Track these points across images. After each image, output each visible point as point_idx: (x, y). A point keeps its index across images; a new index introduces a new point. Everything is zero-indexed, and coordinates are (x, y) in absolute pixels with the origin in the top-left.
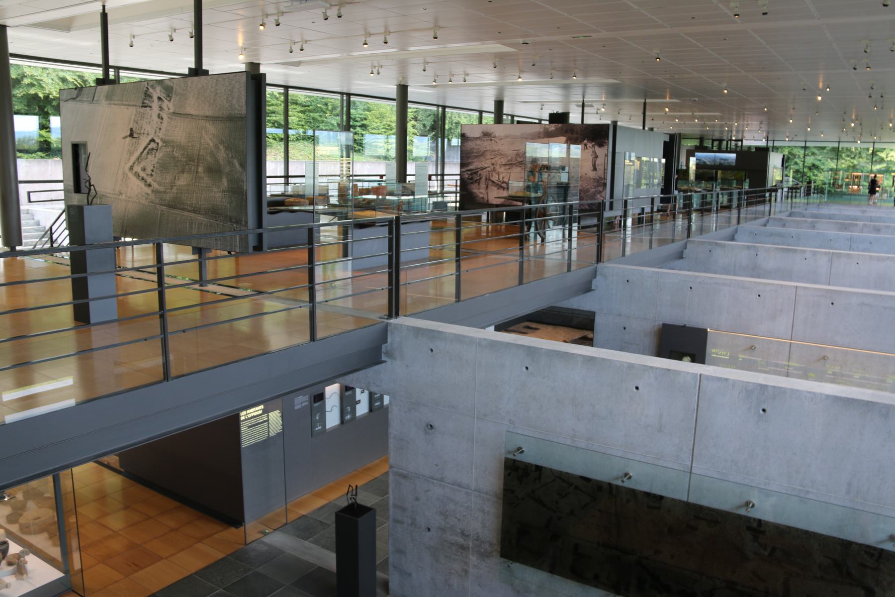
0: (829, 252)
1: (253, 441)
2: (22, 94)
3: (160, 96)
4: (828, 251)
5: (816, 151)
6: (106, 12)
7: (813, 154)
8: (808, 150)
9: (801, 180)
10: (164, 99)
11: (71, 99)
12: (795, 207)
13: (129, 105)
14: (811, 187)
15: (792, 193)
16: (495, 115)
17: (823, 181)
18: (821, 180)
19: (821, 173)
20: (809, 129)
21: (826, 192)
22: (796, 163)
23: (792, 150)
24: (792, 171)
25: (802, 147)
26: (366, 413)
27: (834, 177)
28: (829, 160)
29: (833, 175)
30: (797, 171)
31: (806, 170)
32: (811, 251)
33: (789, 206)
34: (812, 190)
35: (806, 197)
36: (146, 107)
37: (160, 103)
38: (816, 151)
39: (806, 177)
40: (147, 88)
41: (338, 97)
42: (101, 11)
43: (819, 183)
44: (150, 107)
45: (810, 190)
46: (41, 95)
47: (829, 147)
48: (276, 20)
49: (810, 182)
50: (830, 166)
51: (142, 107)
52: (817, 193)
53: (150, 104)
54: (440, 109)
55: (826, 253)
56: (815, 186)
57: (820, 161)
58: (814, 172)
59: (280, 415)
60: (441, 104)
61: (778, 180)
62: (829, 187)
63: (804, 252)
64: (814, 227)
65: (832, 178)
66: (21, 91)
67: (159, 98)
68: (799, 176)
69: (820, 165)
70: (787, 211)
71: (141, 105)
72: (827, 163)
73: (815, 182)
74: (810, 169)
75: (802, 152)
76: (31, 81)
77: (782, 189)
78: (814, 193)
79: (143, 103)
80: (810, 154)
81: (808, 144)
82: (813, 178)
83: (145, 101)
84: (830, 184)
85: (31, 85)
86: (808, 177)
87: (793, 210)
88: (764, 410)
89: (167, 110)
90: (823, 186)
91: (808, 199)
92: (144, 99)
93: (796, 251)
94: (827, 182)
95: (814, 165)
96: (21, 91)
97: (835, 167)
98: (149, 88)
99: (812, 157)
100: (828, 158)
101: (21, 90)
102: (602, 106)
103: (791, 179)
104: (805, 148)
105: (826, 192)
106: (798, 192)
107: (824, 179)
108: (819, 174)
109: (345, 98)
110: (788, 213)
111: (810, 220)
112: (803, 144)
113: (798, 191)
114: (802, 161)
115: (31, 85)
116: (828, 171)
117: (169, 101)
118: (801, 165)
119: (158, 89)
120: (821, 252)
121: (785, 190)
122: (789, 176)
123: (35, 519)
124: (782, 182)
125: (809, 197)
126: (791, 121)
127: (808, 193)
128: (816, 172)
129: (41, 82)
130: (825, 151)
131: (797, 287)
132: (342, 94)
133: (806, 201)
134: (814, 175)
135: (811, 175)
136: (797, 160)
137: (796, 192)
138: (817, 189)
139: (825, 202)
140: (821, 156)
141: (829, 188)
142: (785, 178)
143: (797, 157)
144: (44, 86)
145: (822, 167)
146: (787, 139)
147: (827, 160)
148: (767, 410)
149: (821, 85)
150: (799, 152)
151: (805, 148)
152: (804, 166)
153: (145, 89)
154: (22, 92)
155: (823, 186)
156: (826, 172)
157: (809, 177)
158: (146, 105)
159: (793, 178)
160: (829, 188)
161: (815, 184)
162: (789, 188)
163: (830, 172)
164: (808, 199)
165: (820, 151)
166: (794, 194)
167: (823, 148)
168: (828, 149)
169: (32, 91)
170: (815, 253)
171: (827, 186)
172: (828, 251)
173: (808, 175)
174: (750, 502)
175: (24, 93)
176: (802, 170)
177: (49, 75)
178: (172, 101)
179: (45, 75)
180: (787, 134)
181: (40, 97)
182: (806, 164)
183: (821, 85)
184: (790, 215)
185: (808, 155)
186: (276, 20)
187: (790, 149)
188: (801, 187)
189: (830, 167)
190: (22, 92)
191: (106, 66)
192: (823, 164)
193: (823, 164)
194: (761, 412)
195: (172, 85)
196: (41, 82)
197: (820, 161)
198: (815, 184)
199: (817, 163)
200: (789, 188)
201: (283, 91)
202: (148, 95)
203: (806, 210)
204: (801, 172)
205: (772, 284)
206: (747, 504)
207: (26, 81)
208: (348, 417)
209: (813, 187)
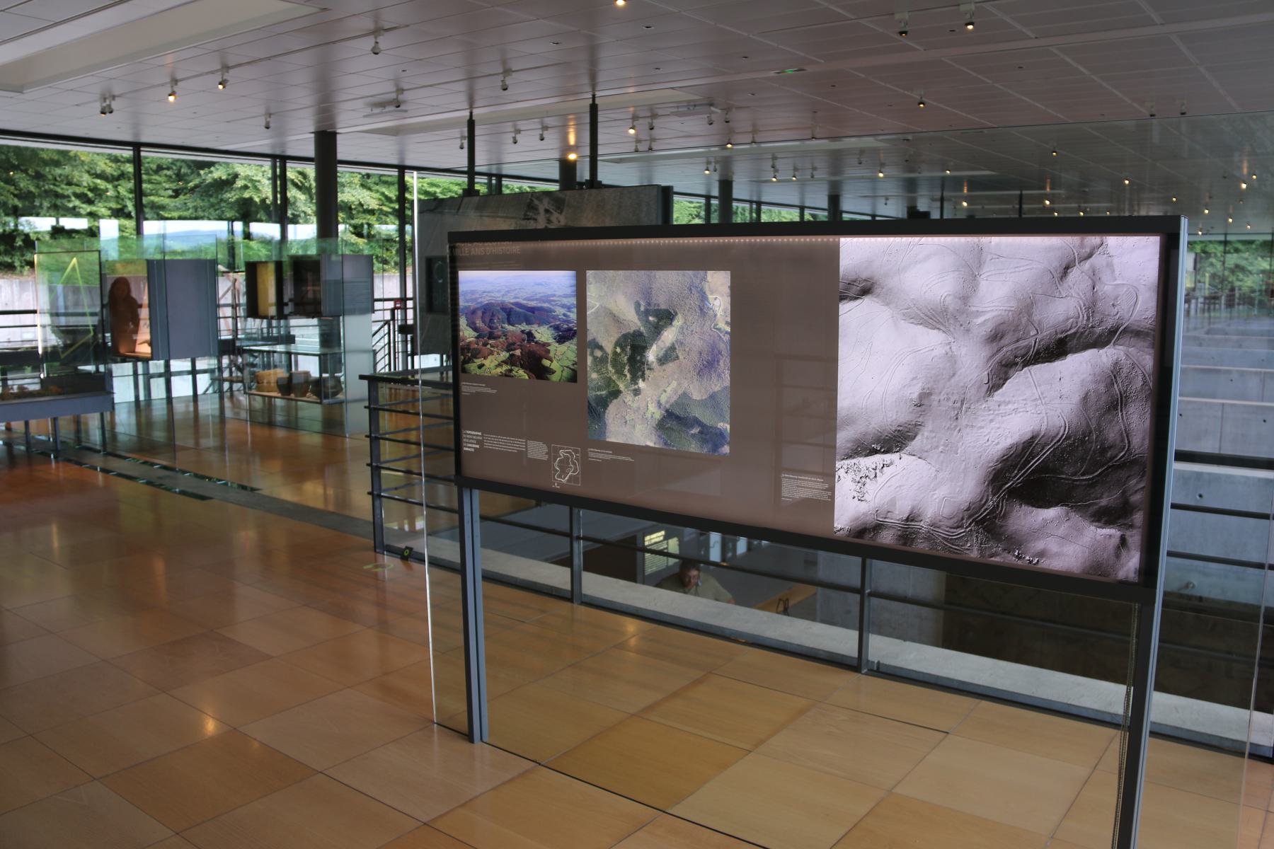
0: (1261, 372)
1: (654, 569)
2: (234, 198)
3: (547, 208)
4: (1259, 370)
5: (1240, 246)
6: (474, 118)
7: (1237, 251)
8: (1228, 245)
9: (1220, 286)
10: (552, 211)
11: (428, 210)
12: (1214, 323)
13: (507, 217)
14: (1234, 295)
15: (1209, 304)
16: (829, 213)
17: (1251, 287)
18: (1248, 287)
19: (1248, 276)
20: (1230, 220)
21: (1256, 302)
22: (1212, 265)
23: (1206, 246)
24: (1207, 275)
25: (1220, 242)
26: (743, 553)
27: (1266, 282)
28: (1260, 259)
29: (1265, 279)
30: (1213, 276)
31: (1226, 273)
32: (1237, 371)
33: (1206, 321)
34: (1237, 301)
35: (1229, 310)
36: (528, 219)
37: (547, 215)
38: (1240, 246)
39: (1226, 282)
40: (531, 200)
41: (747, 206)
42: (468, 118)
43: (1245, 289)
44: (535, 219)
45: (1234, 300)
46: (257, 200)
47: (1258, 240)
48: (649, 123)
49: (1232, 290)
50: (1261, 266)
51: (524, 219)
52: (1244, 304)
53: (535, 217)
54: (754, 206)
55: (1256, 373)
56: (1240, 295)
57: (1246, 259)
58: (1238, 276)
59: (677, 543)
60: (755, 199)
61: (1189, 288)
62: (1261, 295)
63: (1229, 372)
64: (1240, 346)
65: (1264, 283)
66: (233, 194)
67: (547, 211)
68: (1217, 281)
69: (1246, 266)
70: (1203, 328)
71: (523, 217)
72: (1256, 262)
73: (1240, 289)
74: (1232, 272)
75: (1221, 248)
76: (246, 183)
77: (1197, 299)
78: (1239, 304)
79: (525, 215)
80: (1232, 251)
81: (1229, 238)
82: (1237, 284)
83: (528, 213)
84: (1260, 291)
85: (246, 187)
86: (1229, 282)
87: (1212, 326)
88: (1201, 496)
89: (557, 223)
90: (1252, 295)
91: (1231, 312)
92: (527, 211)
93: (1218, 371)
94: (1257, 288)
95: (1237, 266)
96: (233, 194)
97: (1268, 267)
98: (533, 199)
99: (1235, 255)
100: (1259, 255)
101: (233, 193)
102: (630, 123)
103: (1207, 286)
104: (1225, 243)
105: (1256, 302)
106: (1218, 304)
107: (1252, 285)
108: (1246, 279)
109: (494, 182)
110: (1205, 329)
111: (1235, 337)
112: (1222, 238)
113: (1217, 302)
114: (1220, 261)
115: (246, 187)
116: (1258, 274)
117: (561, 213)
118: (1219, 266)
119: (546, 202)
120: (1251, 372)
121: (1201, 300)
122: (1204, 283)
123: (899, 426)
124: (1194, 289)
125: (1233, 309)
126: (1207, 211)
127: (1230, 304)
128: (1241, 276)
129: (257, 184)
130: (1254, 246)
131: (1223, 404)
132: (751, 202)
133: (1228, 315)
134: (1238, 280)
135: (1234, 278)
136: (1213, 260)
137: (1215, 304)
138: (1244, 299)
139: (1255, 315)
140: (1248, 253)
141: (1260, 297)
142: (1199, 285)
143: (1213, 255)
144: (261, 188)
145: (1250, 268)
146: (1200, 233)
147: (1256, 259)
148: (1204, 495)
149: (1245, 171)
150: (1216, 249)
151: (1225, 243)
152: (1224, 269)
153: (528, 201)
154: (235, 195)
155: (1252, 295)
156: (1255, 275)
157: (1232, 282)
158: (529, 217)
159: (1210, 285)
160: (1260, 297)
161: (1240, 292)
162: (1206, 298)
163: (1261, 275)
164: (1231, 312)
165: (1247, 246)
166: (1212, 307)
167: (1251, 242)
168: (1258, 243)
169: (246, 195)
170: (1242, 374)
171: (1257, 294)
172: (1259, 370)
173: (1230, 279)
174: (1191, 583)
175: (237, 197)
176: (1220, 274)
177: (265, 173)
178: (564, 213)
179: (261, 174)
180: (1201, 226)
181: (256, 202)
182: (1226, 265)
183: (1245, 171)
184: (1208, 333)
185: (1229, 252)
186: (649, 123)
187: (1204, 244)
188: (1221, 296)
189: (1262, 268)
190: (235, 195)
191: (471, 172)
192: (1251, 264)
193: (1251, 264)
194: (1198, 497)
195: (563, 196)
196: (257, 184)
197: (1246, 259)
198: (1240, 292)
199: (1243, 263)
200: (1206, 298)
201: (486, 181)
202: (535, 209)
203: (1229, 325)
204: (1219, 277)
205: (1195, 402)
206: (1187, 586)
207: (239, 183)
208: (730, 555)
209: (1237, 295)
